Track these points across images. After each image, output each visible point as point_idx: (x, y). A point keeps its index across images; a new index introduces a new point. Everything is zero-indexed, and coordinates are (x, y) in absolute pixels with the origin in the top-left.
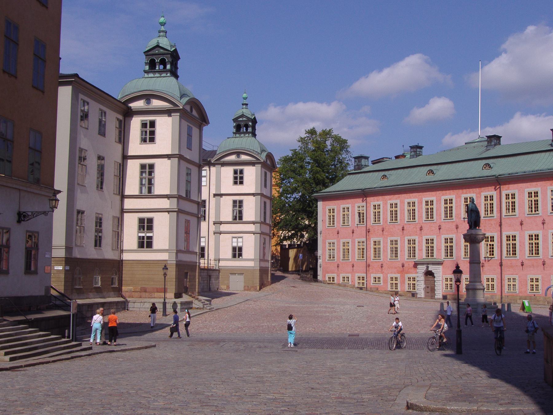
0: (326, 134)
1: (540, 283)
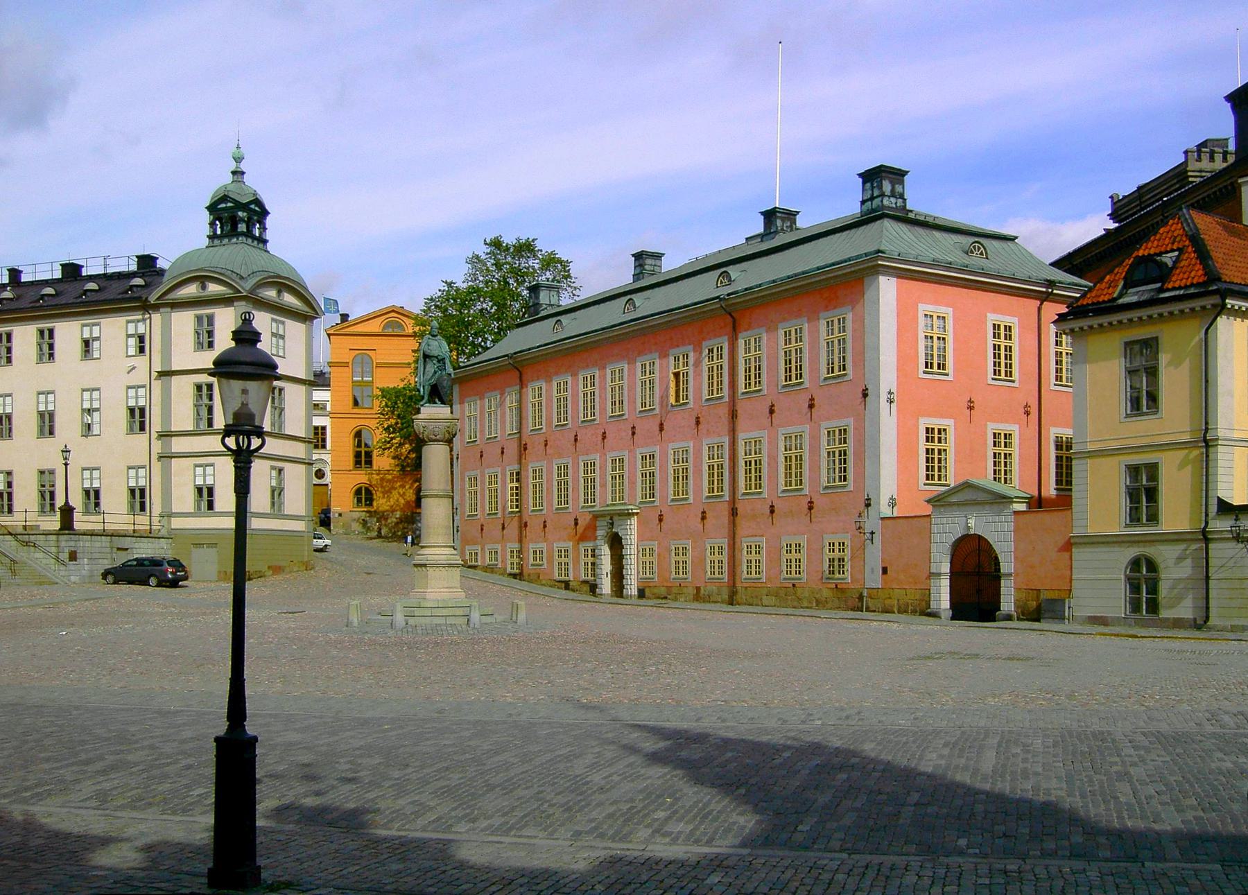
0: (526, 248)
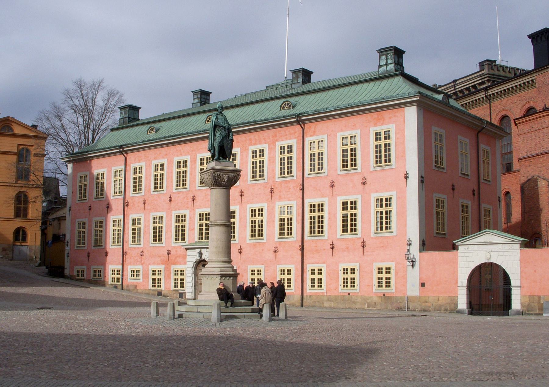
1: (357, 276)
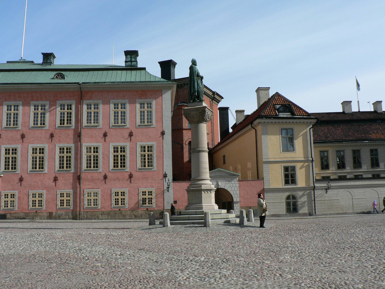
1: (126, 197)
